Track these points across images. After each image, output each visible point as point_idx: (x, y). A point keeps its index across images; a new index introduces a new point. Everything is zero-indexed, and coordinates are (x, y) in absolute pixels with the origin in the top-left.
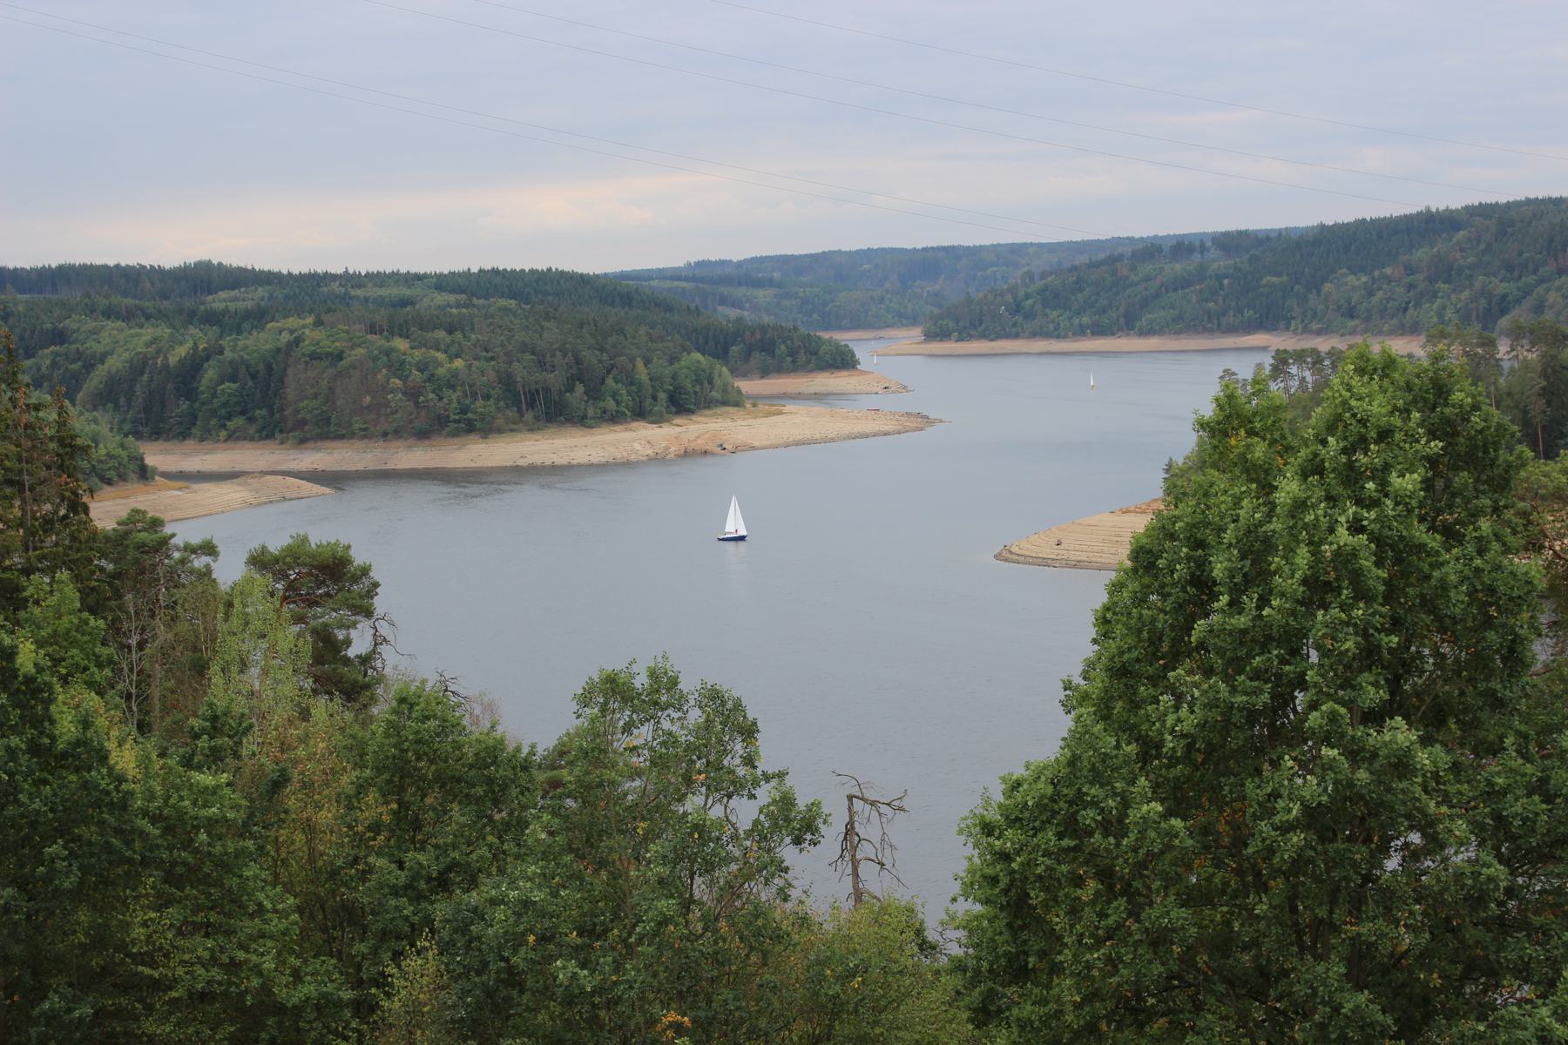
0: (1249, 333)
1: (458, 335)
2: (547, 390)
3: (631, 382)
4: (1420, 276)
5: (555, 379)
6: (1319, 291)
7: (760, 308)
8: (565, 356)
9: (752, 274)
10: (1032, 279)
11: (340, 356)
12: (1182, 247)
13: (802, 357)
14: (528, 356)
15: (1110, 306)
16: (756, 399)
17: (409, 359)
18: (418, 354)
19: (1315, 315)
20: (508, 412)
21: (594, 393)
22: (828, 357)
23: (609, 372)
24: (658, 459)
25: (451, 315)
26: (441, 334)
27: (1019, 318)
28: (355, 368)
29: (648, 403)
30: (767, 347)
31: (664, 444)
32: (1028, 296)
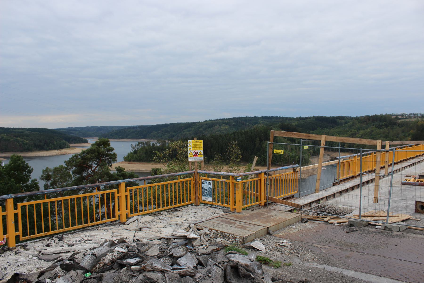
9: (76, 129)
11: (9, 140)
12: (134, 127)
18: (21, 140)
26: (25, 137)
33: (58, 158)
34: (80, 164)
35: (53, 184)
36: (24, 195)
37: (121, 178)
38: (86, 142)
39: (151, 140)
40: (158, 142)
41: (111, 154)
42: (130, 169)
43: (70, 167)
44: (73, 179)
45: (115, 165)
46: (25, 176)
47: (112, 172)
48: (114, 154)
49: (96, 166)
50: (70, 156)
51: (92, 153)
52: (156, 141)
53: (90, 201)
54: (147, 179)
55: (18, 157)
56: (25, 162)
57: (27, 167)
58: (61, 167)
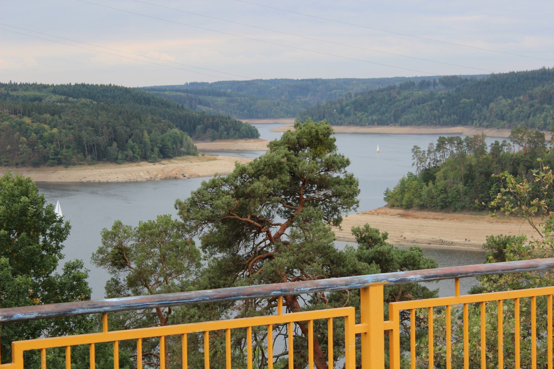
0: (454, 126)
1: (56, 117)
2: (98, 145)
3: (141, 142)
4: (536, 101)
5: (102, 140)
6: (488, 106)
7: (216, 108)
8: (108, 128)
10: (350, 97)
12: (425, 83)
13: (232, 132)
14: (89, 128)
15: (387, 111)
16: (204, 151)
17: (30, 127)
19: (485, 118)
20: (79, 155)
21: (122, 147)
22: (244, 132)
23: (130, 137)
24: (151, 181)
25: (57, 106)
26: (47, 116)
27: (343, 116)
28: (3, 131)
29: (148, 153)
30: (215, 127)
31: (155, 173)
32: (347, 105)
33: (151, 193)
34: (232, 215)
35: (138, 281)
36: (34, 315)
37: (374, 265)
38: (252, 134)
39: (487, 132)
40: (515, 138)
41: (338, 182)
42: (408, 235)
43: (193, 223)
44: (205, 265)
45: (352, 220)
46: (43, 248)
47: (339, 246)
48: (351, 181)
49: (283, 221)
50: (196, 186)
51: (271, 176)
52: (507, 133)
53: (259, 348)
54: (466, 275)
55: (20, 183)
56: (43, 201)
57: (51, 217)
58: (166, 220)
